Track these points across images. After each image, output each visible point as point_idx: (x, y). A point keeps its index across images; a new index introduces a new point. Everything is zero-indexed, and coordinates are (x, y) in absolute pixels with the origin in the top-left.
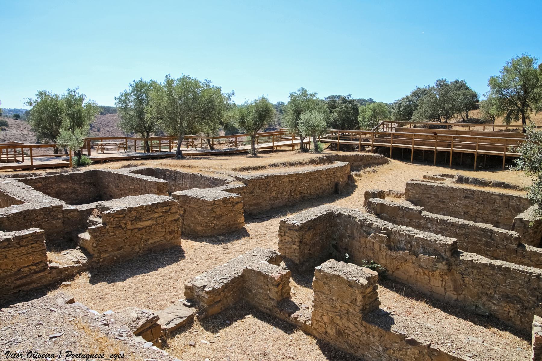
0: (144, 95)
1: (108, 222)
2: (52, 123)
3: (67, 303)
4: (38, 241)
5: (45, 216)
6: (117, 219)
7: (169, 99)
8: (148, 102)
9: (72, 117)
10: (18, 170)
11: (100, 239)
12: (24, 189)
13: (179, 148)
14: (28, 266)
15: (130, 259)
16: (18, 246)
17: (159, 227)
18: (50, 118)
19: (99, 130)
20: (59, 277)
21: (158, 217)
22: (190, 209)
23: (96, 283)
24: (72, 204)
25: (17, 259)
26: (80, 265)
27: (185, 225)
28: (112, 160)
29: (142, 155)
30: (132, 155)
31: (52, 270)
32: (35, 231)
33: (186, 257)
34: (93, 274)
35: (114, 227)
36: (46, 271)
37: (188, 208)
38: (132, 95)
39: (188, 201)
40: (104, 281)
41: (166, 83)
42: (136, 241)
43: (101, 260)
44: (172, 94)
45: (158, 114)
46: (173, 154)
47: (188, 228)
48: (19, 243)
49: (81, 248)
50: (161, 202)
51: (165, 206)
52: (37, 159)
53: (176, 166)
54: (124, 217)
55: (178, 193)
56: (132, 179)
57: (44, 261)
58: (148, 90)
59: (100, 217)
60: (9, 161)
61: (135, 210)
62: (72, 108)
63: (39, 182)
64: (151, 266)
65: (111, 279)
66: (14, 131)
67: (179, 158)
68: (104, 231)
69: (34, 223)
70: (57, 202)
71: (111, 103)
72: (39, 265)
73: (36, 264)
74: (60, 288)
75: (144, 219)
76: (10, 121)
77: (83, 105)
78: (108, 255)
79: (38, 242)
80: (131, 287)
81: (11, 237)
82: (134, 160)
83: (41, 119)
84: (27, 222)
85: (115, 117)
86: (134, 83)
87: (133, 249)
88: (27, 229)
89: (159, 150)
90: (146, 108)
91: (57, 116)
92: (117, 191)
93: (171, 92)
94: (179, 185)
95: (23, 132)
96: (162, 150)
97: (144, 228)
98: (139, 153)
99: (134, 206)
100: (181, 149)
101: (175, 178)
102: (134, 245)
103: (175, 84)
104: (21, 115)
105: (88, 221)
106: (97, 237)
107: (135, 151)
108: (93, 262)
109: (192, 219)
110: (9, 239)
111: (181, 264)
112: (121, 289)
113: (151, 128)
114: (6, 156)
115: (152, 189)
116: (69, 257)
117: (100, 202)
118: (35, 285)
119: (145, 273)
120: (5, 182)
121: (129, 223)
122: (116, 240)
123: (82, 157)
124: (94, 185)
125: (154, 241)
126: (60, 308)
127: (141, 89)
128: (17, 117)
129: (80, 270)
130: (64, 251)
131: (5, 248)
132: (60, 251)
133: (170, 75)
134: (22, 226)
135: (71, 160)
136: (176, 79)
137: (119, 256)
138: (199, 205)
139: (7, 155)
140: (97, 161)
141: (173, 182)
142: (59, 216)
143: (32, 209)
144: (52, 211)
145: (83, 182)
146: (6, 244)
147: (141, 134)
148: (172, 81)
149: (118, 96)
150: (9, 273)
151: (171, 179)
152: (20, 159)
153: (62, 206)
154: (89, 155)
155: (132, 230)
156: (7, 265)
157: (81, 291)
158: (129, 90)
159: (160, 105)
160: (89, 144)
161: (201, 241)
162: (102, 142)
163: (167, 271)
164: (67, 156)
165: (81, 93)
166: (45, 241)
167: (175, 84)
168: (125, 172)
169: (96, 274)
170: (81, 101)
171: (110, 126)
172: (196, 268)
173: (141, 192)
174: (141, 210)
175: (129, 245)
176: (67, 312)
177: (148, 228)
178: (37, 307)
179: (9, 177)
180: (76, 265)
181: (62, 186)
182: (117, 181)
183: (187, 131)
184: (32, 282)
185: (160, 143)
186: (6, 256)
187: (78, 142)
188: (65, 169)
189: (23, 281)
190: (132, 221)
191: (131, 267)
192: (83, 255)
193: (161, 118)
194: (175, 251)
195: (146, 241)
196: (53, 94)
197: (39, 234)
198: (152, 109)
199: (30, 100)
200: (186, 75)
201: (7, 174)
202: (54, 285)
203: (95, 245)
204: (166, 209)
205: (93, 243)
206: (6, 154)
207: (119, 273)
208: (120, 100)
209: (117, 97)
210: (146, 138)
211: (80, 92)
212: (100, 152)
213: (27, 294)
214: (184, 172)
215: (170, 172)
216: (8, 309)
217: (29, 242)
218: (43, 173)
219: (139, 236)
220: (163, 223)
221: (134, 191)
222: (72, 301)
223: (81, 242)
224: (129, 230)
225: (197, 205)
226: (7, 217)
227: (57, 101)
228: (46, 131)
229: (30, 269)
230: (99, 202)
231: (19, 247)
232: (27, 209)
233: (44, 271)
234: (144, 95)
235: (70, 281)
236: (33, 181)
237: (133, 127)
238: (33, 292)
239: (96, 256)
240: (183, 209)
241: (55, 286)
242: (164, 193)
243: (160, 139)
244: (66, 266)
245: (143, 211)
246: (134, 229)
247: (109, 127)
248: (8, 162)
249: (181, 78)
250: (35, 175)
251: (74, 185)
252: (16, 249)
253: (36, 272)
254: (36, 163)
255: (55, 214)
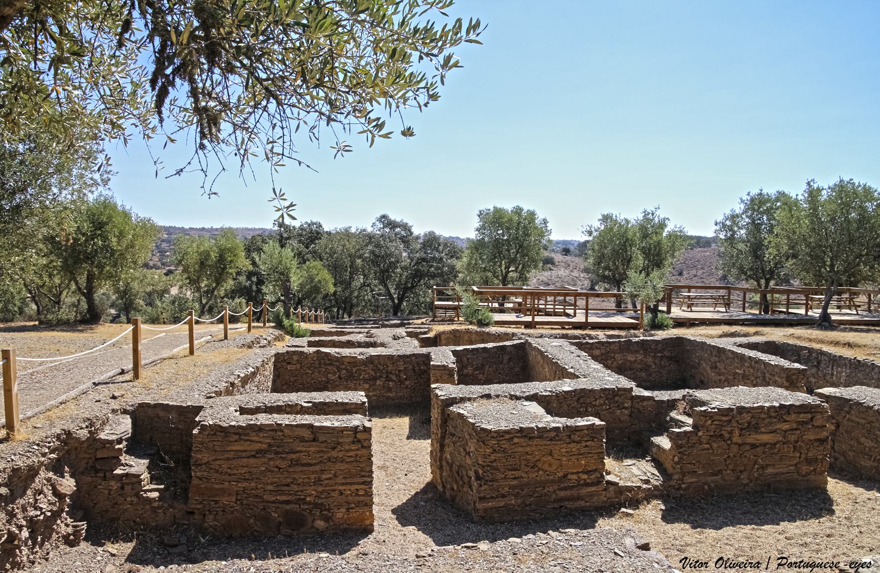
0: (765, 218)
1: (702, 426)
2: (618, 261)
3: (639, 547)
4: (596, 438)
5: (607, 402)
6: (717, 422)
7: (812, 222)
8: (772, 226)
9: (646, 252)
10: (567, 327)
11: (686, 451)
12: (579, 356)
13: (825, 308)
14: (577, 473)
15: (731, 495)
16: (568, 441)
17: (788, 447)
18: (616, 254)
19: (681, 274)
20: (617, 500)
21: (790, 430)
22: (850, 424)
23: (673, 522)
24: (646, 388)
25: (565, 459)
26: (650, 487)
27: (835, 451)
28: (704, 322)
29: (755, 317)
30: (738, 316)
31: (609, 486)
32: (593, 422)
33: (837, 512)
34: (669, 506)
35: (711, 436)
36: (600, 486)
37: (845, 422)
38: (744, 216)
39: (846, 409)
40: (685, 522)
41: (806, 195)
42: (744, 465)
43: (683, 486)
44: (818, 214)
45: (789, 249)
46: (812, 320)
47: (842, 459)
48: (569, 436)
49: (654, 460)
50: (798, 403)
51: (804, 413)
52: (594, 313)
53: (822, 342)
54: (730, 421)
55: (827, 391)
56: (742, 357)
57: (600, 469)
58: (773, 209)
59: (689, 415)
60: (556, 314)
61: (749, 412)
62: (648, 239)
63: (597, 348)
64: (768, 515)
65: (696, 521)
66: (562, 272)
67: (826, 329)
68: (694, 439)
69: (590, 410)
70: (624, 382)
71: (709, 232)
72: (591, 475)
73: (587, 472)
74: (617, 517)
75: (763, 430)
76: (558, 257)
77: (664, 234)
78: (696, 480)
79: (595, 440)
80: (730, 543)
81: (560, 425)
82: (741, 325)
83: (603, 254)
84: (581, 407)
85: (708, 254)
86: (749, 198)
87: (738, 478)
88: (582, 418)
89: (785, 310)
90: (767, 238)
91: (626, 251)
92: (713, 374)
93: (815, 209)
94: (824, 376)
95: (572, 274)
96: (790, 310)
97: (761, 445)
98: (750, 314)
99: (748, 405)
100: (829, 311)
101: (819, 363)
102: (741, 472)
103: (825, 197)
104: (572, 248)
105: (668, 418)
106: (681, 448)
107: (744, 311)
108: (670, 486)
109: (852, 443)
110: (558, 428)
111: (824, 523)
112: (713, 543)
113: (773, 272)
114: (552, 307)
115: (777, 378)
116: (635, 470)
117: (691, 391)
118: (583, 503)
119: (756, 524)
120: (553, 344)
121: (737, 432)
122: (712, 458)
123: (659, 315)
124: (677, 360)
125: (777, 471)
126: (629, 554)
127: (759, 208)
128: (566, 251)
129: (650, 495)
130: (628, 460)
131: (551, 440)
132: (622, 458)
133: (816, 180)
134: (574, 411)
135: (642, 318)
136: (826, 187)
137: (713, 485)
138: (870, 419)
139: (554, 305)
140: (680, 323)
141: (814, 370)
142: (626, 405)
143: (590, 388)
144: (618, 395)
145: (659, 355)
146: (553, 434)
147: (756, 283)
148: (819, 190)
149: (720, 218)
150: (552, 477)
151: (810, 364)
152: (571, 312)
153: (632, 388)
154: (669, 312)
155: (740, 445)
156: (550, 465)
157: (647, 529)
158: (739, 208)
159: (794, 233)
160: (669, 295)
161: (869, 489)
162: (689, 292)
163: (797, 531)
164: (636, 311)
165: (662, 216)
166: (604, 440)
167: (824, 195)
168: (727, 344)
169: (673, 508)
170: (662, 228)
171: (700, 266)
172: (856, 539)
173: (755, 382)
174: (760, 413)
175: (732, 470)
176: (639, 564)
177: (768, 446)
178: (596, 543)
179: (556, 338)
180: (645, 486)
181: (629, 358)
182: (714, 359)
183: (844, 278)
184: (579, 498)
185: (788, 299)
186: (551, 451)
187: (656, 292)
188: (632, 331)
189: (568, 493)
190: (741, 429)
191: (732, 509)
192: (656, 472)
193: (795, 256)
194: (815, 497)
195: (763, 468)
196: (622, 218)
197: (598, 428)
198: (779, 240)
199: (590, 227)
200: (846, 179)
201: (554, 332)
202: (609, 510)
203: (676, 459)
204: (803, 417)
205: (674, 456)
206: (552, 303)
207: (710, 514)
208: (724, 226)
209: (718, 221)
210: (763, 288)
211: (661, 214)
212: (685, 309)
213: (571, 515)
214: (838, 354)
215: (809, 352)
216: (557, 533)
217: (583, 437)
218: (601, 335)
219: (752, 457)
220: (797, 442)
221: (743, 378)
222: (645, 547)
223: (654, 450)
224: (736, 444)
225: (864, 419)
226: (557, 395)
227: (627, 228)
228: (607, 273)
229: (579, 477)
230: (687, 390)
231: (570, 443)
232: (583, 387)
233: (598, 485)
234: (765, 218)
235: (633, 509)
236: (589, 346)
237: (742, 270)
238: (579, 513)
239: (676, 477)
240: (834, 421)
241: (611, 512)
242: (798, 387)
243: (788, 292)
244: (629, 484)
245: (763, 416)
246: (745, 443)
247: (697, 269)
248: (555, 315)
249: (835, 185)
250: (591, 337)
251: (646, 357)
252: (565, 445)
253: (587, 485)
254: (592, 319)
255: (620, 400)
